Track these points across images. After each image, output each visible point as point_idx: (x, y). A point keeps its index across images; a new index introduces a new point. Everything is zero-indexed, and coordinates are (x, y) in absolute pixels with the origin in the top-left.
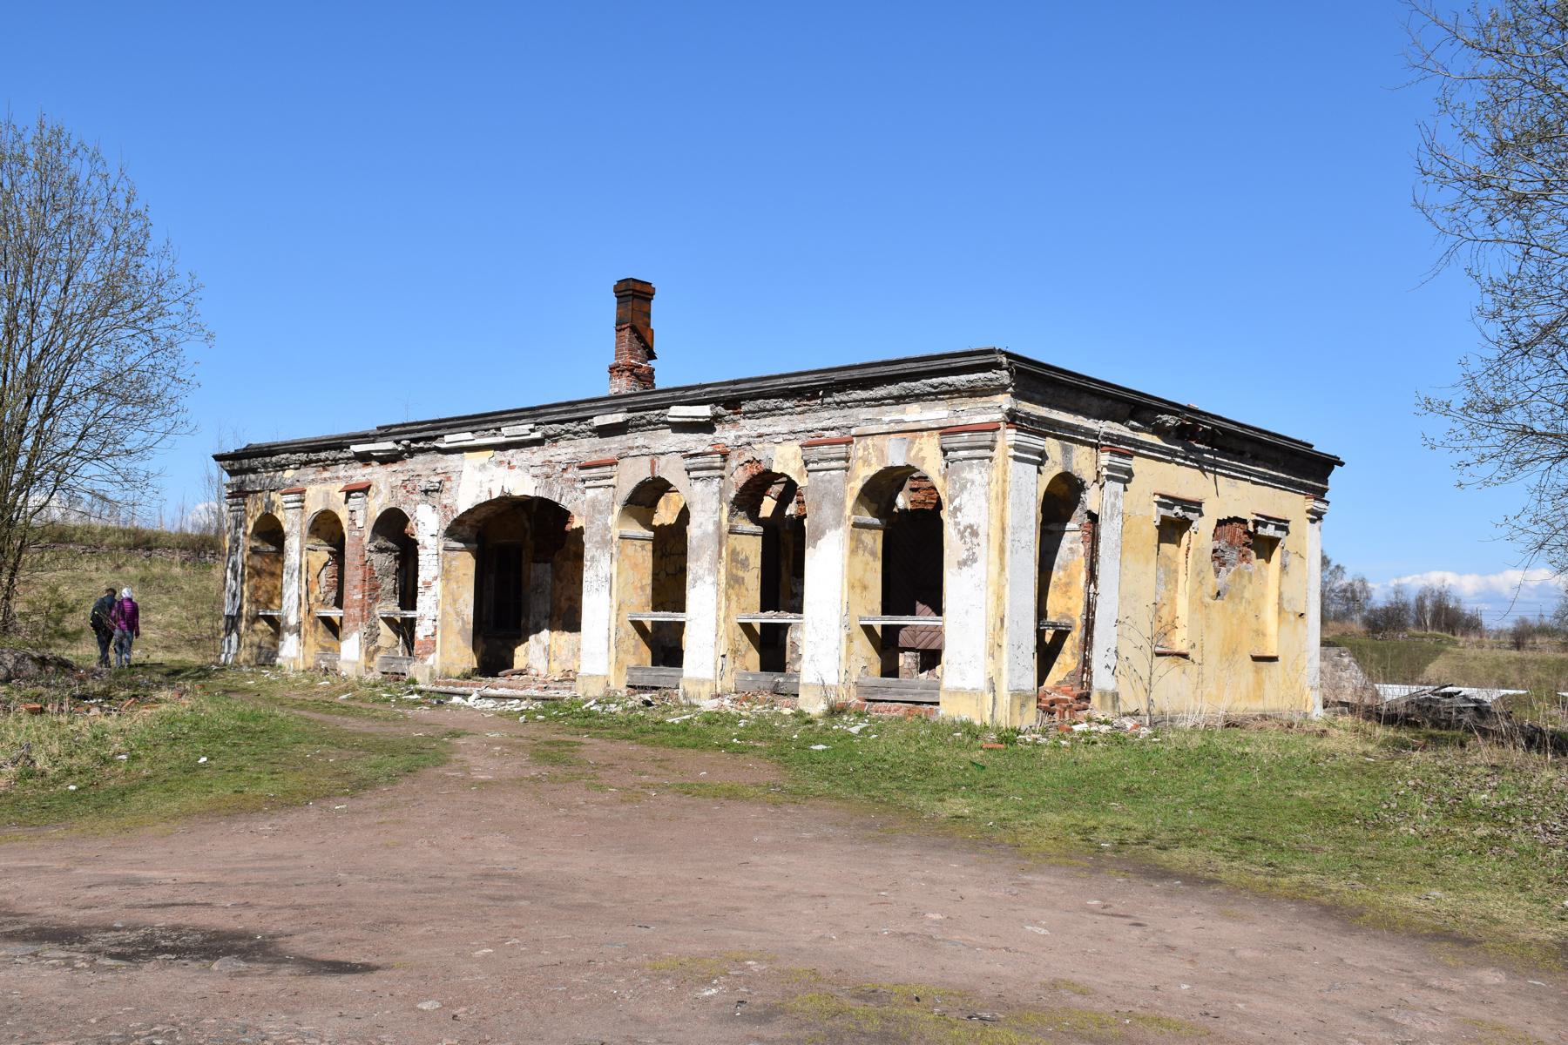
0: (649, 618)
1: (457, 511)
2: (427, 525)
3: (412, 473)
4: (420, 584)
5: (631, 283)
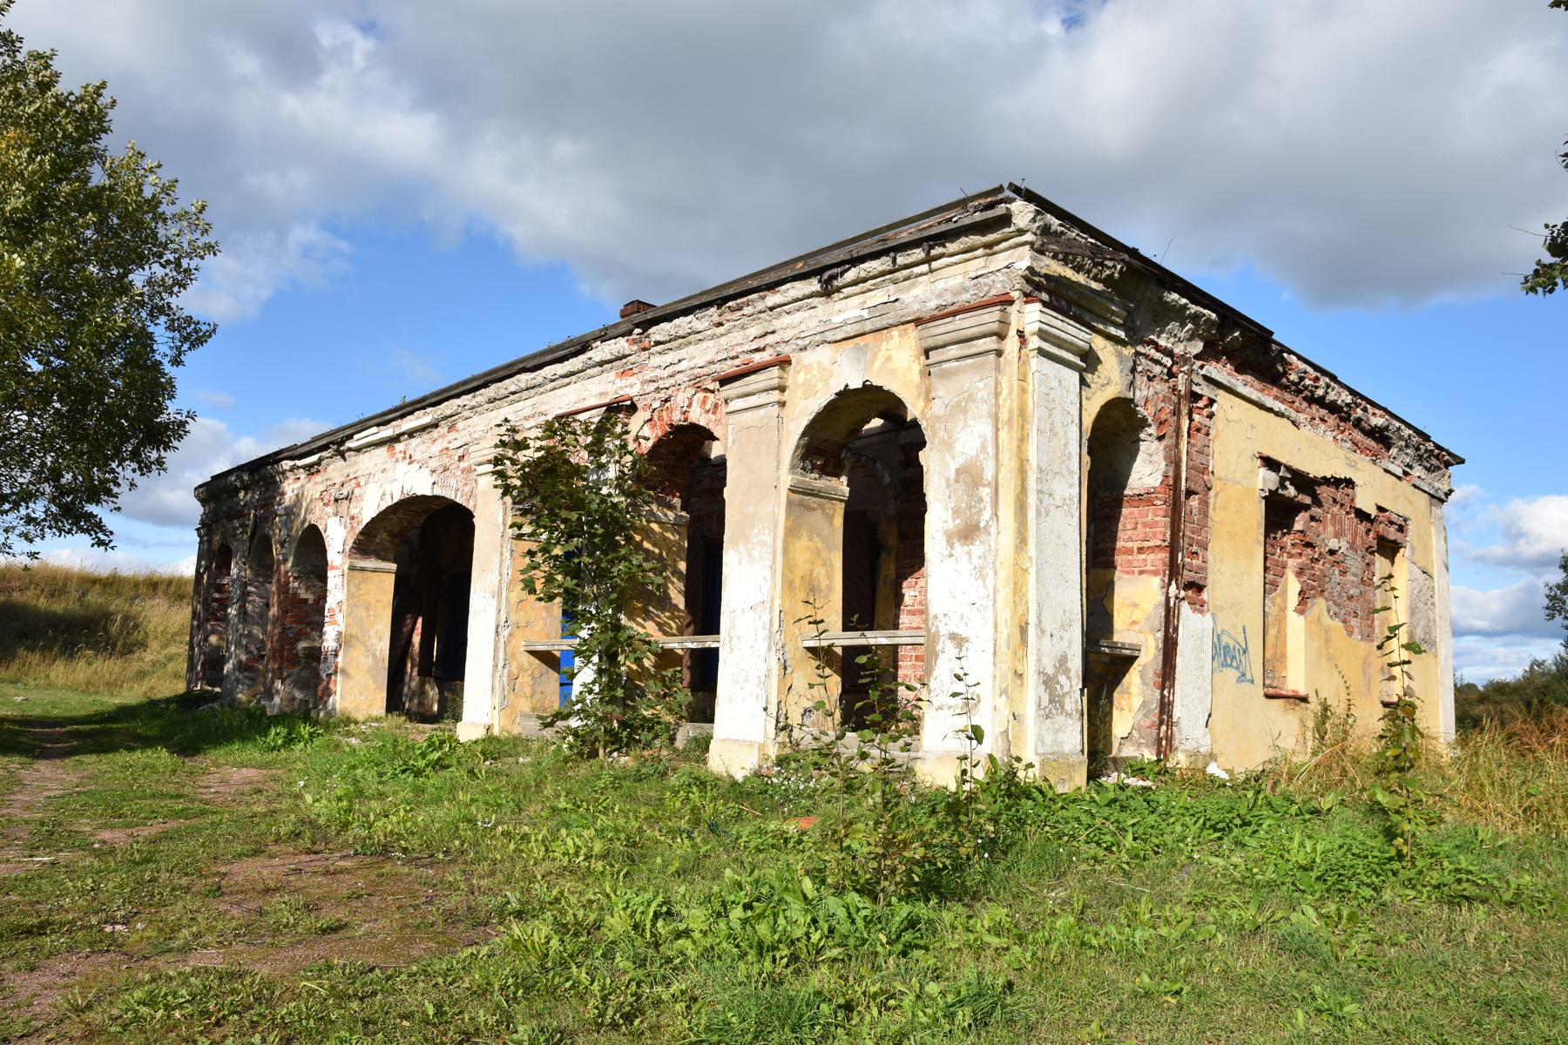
0: (842, 639)
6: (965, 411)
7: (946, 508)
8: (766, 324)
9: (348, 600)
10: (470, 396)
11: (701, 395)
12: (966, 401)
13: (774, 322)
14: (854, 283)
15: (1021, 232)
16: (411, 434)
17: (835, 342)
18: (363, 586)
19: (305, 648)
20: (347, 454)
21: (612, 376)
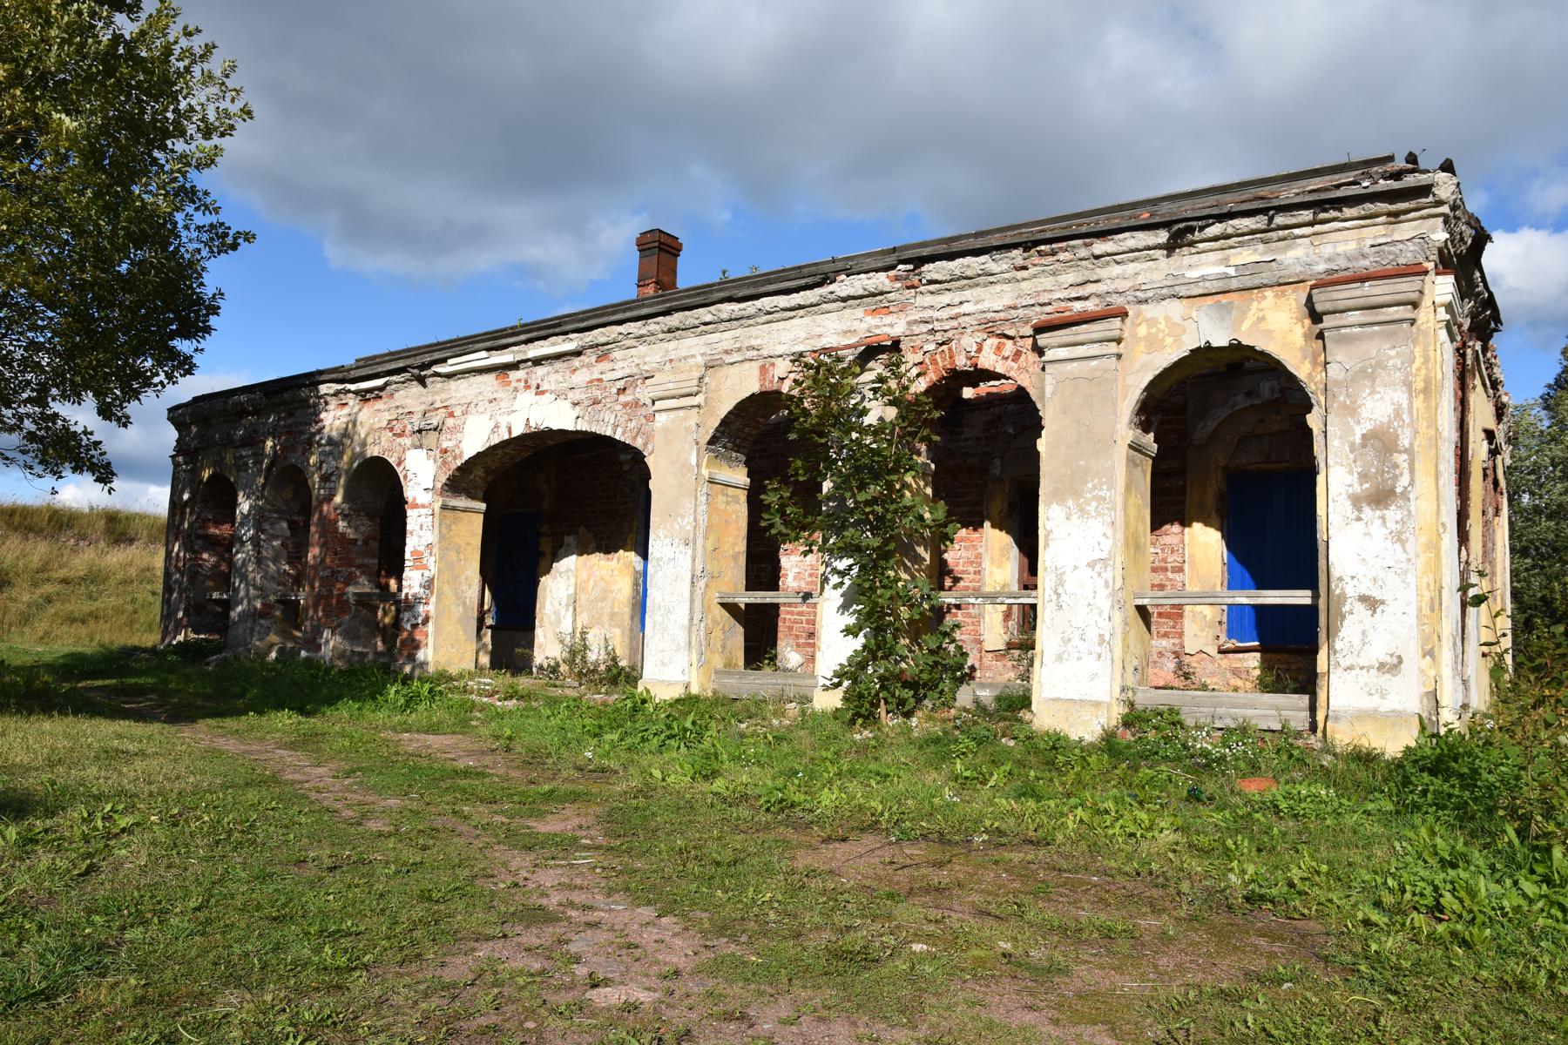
0: (745, 598)
1: (461, 455)
3: (400, 411)
4: (407, 556)
5: (657, 234)
6: (1373, 378)
7: (1351, 472)
8: (1087, 273)
9: (440, 542)
10: (639, 324)
11: (994, 341)
12: (1374, 367)
13: (1098, 270)
14: (1215, 239)
15: (1439, 203)
16: (537, 362)
17: (1189, 297)
18: (453, 527)
19: (355, 594)
20: (428, 381)
21: (859, 312)
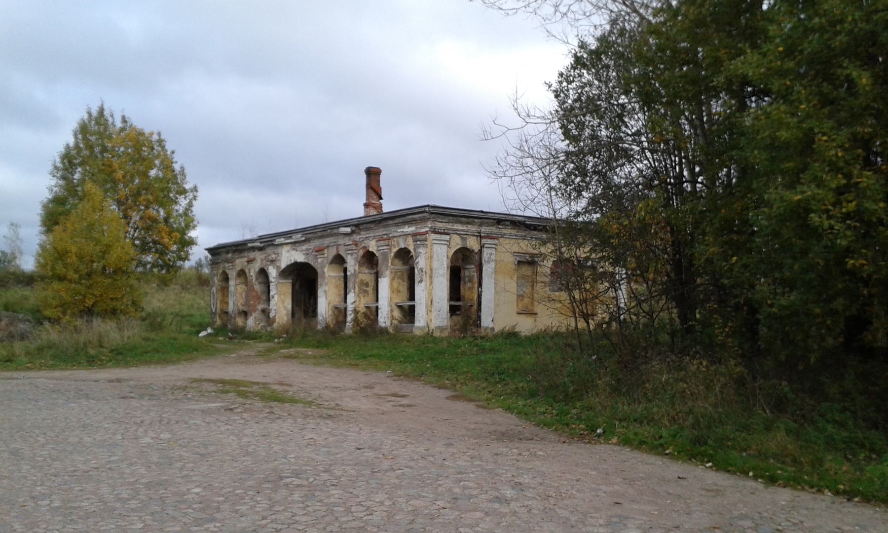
2: (273, 272)
